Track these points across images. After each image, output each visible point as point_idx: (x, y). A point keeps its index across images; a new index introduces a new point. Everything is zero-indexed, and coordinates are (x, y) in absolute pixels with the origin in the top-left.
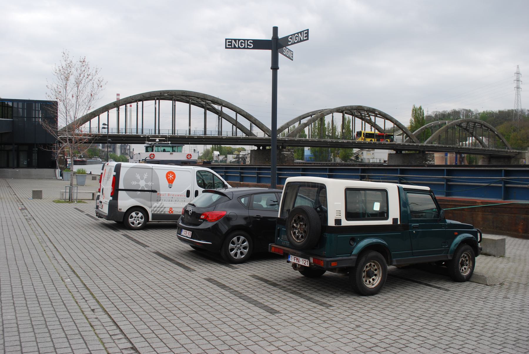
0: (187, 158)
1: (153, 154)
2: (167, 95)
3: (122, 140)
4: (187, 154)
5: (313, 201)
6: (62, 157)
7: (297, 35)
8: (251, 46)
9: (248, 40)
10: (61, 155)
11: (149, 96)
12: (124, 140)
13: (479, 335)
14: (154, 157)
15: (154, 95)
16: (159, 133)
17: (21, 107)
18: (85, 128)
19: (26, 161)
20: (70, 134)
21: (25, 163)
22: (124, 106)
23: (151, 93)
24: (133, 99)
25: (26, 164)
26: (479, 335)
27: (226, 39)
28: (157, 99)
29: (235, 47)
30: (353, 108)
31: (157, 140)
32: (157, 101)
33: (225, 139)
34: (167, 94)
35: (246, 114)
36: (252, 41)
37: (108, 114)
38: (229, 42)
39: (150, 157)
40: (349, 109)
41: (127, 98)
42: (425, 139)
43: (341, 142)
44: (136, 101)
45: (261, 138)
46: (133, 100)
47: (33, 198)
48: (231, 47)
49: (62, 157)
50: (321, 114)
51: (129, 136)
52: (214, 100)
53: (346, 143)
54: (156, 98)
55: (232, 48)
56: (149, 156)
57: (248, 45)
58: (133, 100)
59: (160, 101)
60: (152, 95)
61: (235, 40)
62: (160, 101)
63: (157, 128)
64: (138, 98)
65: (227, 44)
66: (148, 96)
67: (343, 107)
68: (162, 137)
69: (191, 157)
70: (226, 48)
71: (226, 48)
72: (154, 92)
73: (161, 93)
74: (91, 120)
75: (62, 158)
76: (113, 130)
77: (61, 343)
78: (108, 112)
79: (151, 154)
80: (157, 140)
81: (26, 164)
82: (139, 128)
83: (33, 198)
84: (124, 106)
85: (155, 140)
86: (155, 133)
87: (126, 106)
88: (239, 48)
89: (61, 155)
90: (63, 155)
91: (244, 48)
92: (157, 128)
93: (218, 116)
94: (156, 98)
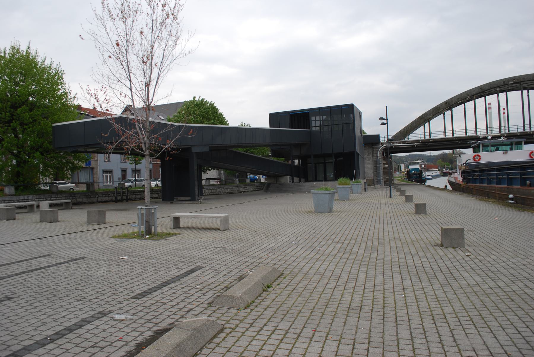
0: (530, 156)
1: (479, 156)
2: (512, 82)
3: (457, 144)
4: (530, 152)
10: (387, 166)
11: (489, 88)
13: (96, 326)
14: (480, 159)
15: (495, 86)
17: (313, 121)
19: (333, 174)
20: (397, 142)
21: (332, 176)
24: (469, 94)
25: (333, 176)
26: (96, 326)
28: (525, 89)
32: (525, 92)
34: (512, 81)
37: (444, 117)
39: (474, 160)
41: (461, 94)
44: (497, 93)
45: (497, 135)
46: (468, 95)
51: (465, 138)
56: (472, 158)
58: (468, 95)
59: (508, 93)
62: (508, 93)
63: (527, 122)
64: (474, 93)
68: (417, 142)
73: (504, 82)
74: (430, 121)
76: (460, 133)
77: (436, 348)
78: (444, 114)
79: (476, 155)
81: (333, 176)
82: (526, 123)
92: (527, 122)
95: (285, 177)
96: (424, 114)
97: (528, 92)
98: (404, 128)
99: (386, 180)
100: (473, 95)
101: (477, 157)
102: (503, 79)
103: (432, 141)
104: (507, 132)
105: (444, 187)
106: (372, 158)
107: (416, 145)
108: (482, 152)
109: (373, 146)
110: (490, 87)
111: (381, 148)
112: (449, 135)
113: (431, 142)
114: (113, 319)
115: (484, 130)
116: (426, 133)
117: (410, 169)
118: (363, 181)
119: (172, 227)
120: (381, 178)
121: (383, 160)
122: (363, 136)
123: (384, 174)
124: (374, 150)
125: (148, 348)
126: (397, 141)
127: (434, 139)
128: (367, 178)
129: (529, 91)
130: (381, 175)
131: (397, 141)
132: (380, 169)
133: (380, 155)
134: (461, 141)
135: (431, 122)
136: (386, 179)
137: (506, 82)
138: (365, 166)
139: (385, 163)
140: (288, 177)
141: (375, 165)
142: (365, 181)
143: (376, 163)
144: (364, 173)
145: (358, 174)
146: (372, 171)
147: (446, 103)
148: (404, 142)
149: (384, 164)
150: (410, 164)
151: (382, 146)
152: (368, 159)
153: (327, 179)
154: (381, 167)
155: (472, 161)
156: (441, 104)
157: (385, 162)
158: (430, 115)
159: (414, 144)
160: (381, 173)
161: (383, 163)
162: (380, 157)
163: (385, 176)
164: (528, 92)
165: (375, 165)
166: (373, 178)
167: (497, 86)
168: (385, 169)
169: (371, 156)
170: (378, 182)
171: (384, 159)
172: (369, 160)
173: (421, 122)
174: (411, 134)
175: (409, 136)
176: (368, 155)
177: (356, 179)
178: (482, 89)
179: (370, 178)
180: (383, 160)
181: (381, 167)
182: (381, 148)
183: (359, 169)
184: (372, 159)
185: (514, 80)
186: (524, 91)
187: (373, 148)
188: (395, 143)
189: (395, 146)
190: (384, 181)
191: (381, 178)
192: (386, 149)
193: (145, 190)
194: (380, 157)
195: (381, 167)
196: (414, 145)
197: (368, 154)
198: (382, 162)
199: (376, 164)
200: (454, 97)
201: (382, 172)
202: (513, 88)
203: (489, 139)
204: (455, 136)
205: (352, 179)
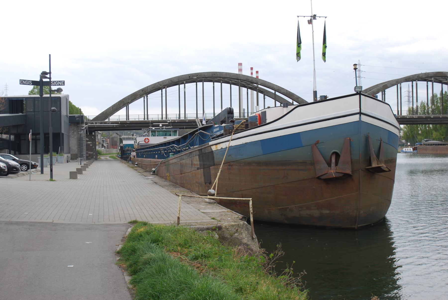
1: (148, 139)
2: (196, 78)
5: (393, 202)
6: (91, 144)
7: (27, 81)
8: (31, 83)
9: (30, 81)
10: (90, 143)
11: (178, 81)
12: (429, 121)
14: (149, 141)
16: (147, 119)
18: (115, 117)
22: (161, 90)
23: (179, 78)
27: (20, 80)
29: (24, 84)
30: (430, 76)
31: (161, 125)
32: (430, 84)
33: (177, 122)
35: (286, 92)
36: (31, 81)
38: (21, 81)
39: (145, 141)
40: (424, 77)
41: (155, 84)
42: (196, 123)
43: (409, 118)
44: (412, 81)
46: (161, 85)
47: (71, 178)
48: (22, 84)
49: (91, 144)
50: (384, 86)
51: (184, 121)
52: (249, 80)
53: (416, 118)
54: (185, 82)
55: (23, 84)
57: (30, 83)
58: (161, 85)
59: (198, 83)
60: (180, 79)
61: (24, 80)
62: (198, 83)
64: (166, 84)
65: (21, 82)
66: (176, 80)
67: (415, 75)
69: (149, 141)
70: (20, 84)
71: (20, 84)
72: (182, 76)
73: (190, 77)
75: (91, 145)
79: (145, 139)
80: (161, 125)
83: (71, 178)
84: (161, 90)
85: (158, 126)
86: (162, 118)
87: (162, 91)
88: (26, 84)
89: (90, 143)
90: (92, 143)
91: (28, 84)
93: (263, 95)
94: (185, 82)
95: (5, 150)
96: (124, 99)
97: (427, 83)
98: (106, 110)
99: (88, 155)
100: (165, 86)
101: (147, 139)
102: (189, 74)
103: (129, 123)
104: (146, 119)
105: (206, 184)
106: (76, 135)
107: (116, 126)
108: (151, 136)
109: (78, 124)
110: (179, 80)
111: (85, 127)
112: (182, 118)
113: (128, 124)
114: (230, 218)
115: (195, 116)
116: (163, 115)
117: (124, 144)
118: (65, 156)
119: (69, 178)
120: (84, 153)
121: (86, 137)
122: (69, 116)
123: (87, 150)
124: (78, 129)
125: (392, 209)
126: (100, 121)
127: (130, 121)
128: (71, 153)
129: (428, 82)
130: (84, 151)
131: (100, 121)
132: (83, 145)
133: (83, 133)
134: (127, 125)
135: (130, 105)
136: (89, 154)
137: (191, 77)
138: (70, 142)
139: (88, 140)
140: (7, 150)
141: (79, 142)
142: (69, 155)
143: (80, 140)
144: (69, 148)
145: (62, 150)
146: (76, 147)
147: (143, 90)
148: (106, 123)
149: (87, 141)
150: (124, 139)
151: (86, 124)
152: (73, 136)
153: (38, 153)
154: (84, 143)
155: (144, 142)
156: (139, 91)
157: (88, 139)
158: (129, 100)
159: (114, 125)
160: (84, 149)
161: (86, 140)
162: (84, 135)
163: (88, 151)
164: (427, 83)
165: (79, 142)
166: (77, 153)
167: (184, 79)
168: (88, 145)
169: (75, 133)
170: (81, 156)
171: (87, 136)
172: (74, 137)
173: (121, 105)
174: (112, 116)
175: (110, 117)
176: (73, 133)
177: (61, 152)
178: (172, 81)
179: (74, 153)
180: (86, 137)
181: (84, 143)
182: (85, 127)
183: (63, 145)
184: (76, 136)
185: (197, 76)
186: (414, 82)
187: (78, 127)
188: (98, 123)
189: (97, 126)
190: (87, 156)
191: (84, 153)
192: (90, 128)
193: (171, 136)
194: (84, 135)
195: (84, 144)
196: (114, 126)
197: (73, 132)
198: (85, 139)
199: (79, 140)
200: (149, 86)
201: (85, 148)
202: (236, 82)
203: (160, 127)
204: (146, 119)
205: (57, 153)
